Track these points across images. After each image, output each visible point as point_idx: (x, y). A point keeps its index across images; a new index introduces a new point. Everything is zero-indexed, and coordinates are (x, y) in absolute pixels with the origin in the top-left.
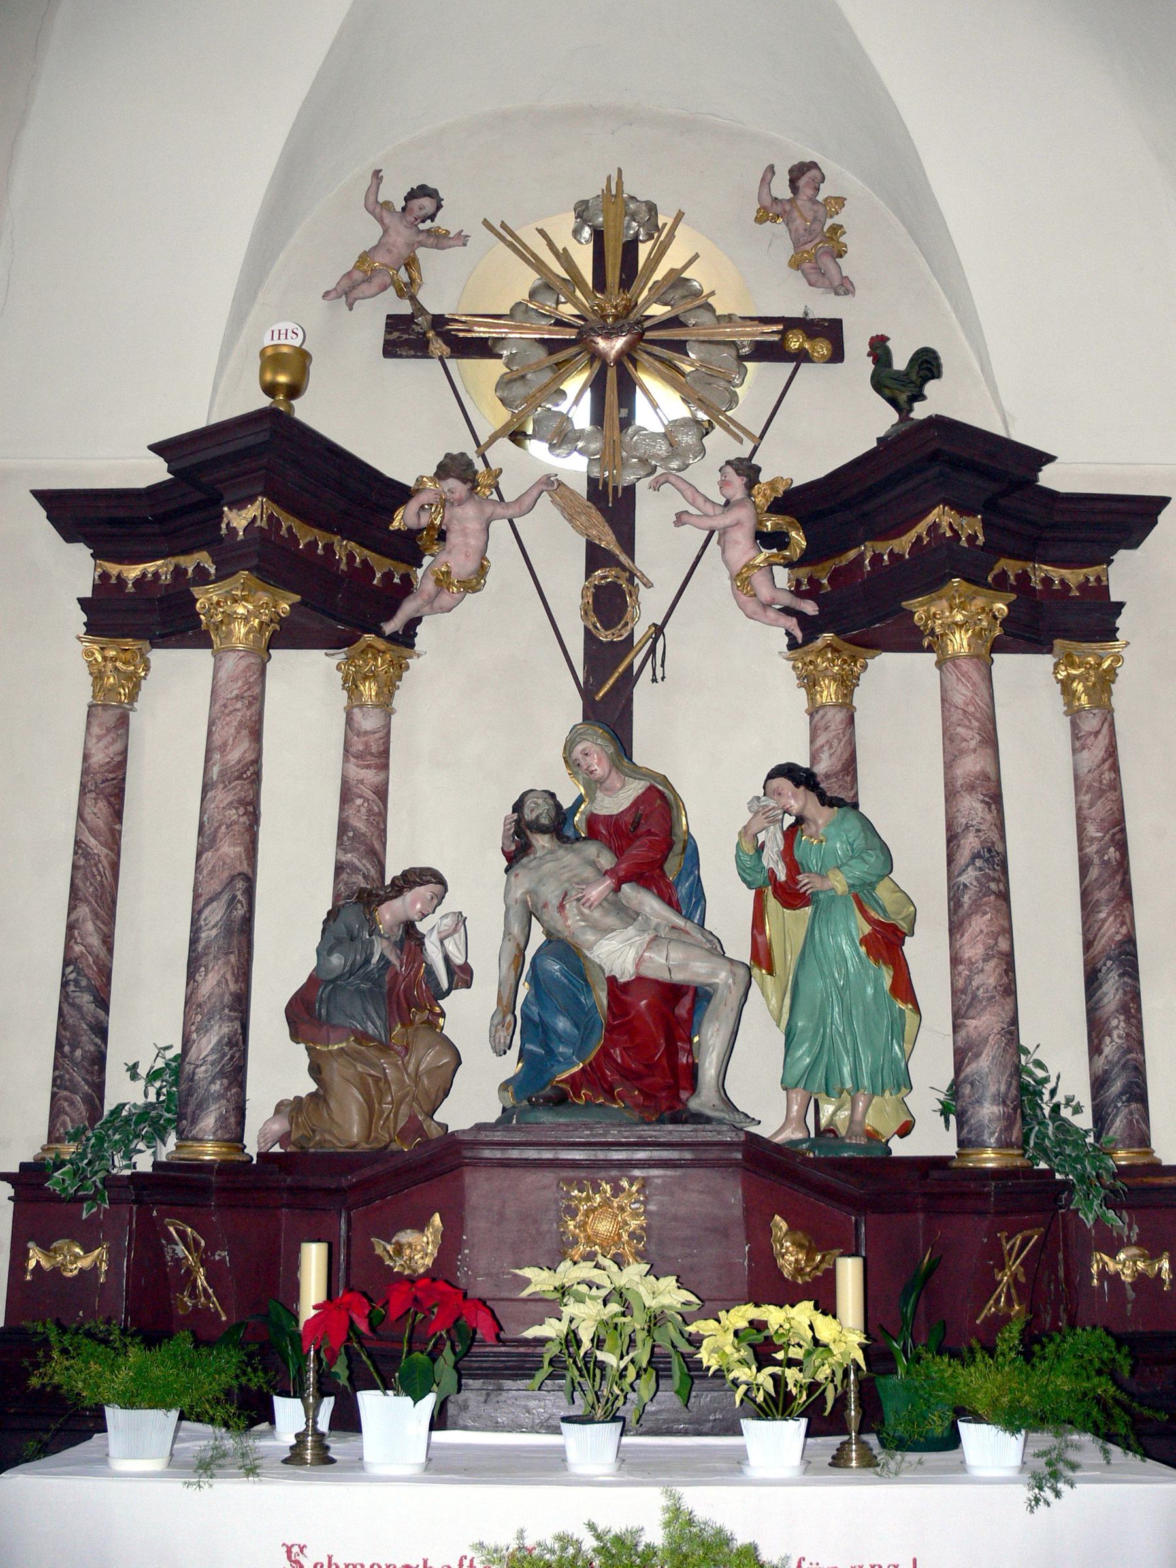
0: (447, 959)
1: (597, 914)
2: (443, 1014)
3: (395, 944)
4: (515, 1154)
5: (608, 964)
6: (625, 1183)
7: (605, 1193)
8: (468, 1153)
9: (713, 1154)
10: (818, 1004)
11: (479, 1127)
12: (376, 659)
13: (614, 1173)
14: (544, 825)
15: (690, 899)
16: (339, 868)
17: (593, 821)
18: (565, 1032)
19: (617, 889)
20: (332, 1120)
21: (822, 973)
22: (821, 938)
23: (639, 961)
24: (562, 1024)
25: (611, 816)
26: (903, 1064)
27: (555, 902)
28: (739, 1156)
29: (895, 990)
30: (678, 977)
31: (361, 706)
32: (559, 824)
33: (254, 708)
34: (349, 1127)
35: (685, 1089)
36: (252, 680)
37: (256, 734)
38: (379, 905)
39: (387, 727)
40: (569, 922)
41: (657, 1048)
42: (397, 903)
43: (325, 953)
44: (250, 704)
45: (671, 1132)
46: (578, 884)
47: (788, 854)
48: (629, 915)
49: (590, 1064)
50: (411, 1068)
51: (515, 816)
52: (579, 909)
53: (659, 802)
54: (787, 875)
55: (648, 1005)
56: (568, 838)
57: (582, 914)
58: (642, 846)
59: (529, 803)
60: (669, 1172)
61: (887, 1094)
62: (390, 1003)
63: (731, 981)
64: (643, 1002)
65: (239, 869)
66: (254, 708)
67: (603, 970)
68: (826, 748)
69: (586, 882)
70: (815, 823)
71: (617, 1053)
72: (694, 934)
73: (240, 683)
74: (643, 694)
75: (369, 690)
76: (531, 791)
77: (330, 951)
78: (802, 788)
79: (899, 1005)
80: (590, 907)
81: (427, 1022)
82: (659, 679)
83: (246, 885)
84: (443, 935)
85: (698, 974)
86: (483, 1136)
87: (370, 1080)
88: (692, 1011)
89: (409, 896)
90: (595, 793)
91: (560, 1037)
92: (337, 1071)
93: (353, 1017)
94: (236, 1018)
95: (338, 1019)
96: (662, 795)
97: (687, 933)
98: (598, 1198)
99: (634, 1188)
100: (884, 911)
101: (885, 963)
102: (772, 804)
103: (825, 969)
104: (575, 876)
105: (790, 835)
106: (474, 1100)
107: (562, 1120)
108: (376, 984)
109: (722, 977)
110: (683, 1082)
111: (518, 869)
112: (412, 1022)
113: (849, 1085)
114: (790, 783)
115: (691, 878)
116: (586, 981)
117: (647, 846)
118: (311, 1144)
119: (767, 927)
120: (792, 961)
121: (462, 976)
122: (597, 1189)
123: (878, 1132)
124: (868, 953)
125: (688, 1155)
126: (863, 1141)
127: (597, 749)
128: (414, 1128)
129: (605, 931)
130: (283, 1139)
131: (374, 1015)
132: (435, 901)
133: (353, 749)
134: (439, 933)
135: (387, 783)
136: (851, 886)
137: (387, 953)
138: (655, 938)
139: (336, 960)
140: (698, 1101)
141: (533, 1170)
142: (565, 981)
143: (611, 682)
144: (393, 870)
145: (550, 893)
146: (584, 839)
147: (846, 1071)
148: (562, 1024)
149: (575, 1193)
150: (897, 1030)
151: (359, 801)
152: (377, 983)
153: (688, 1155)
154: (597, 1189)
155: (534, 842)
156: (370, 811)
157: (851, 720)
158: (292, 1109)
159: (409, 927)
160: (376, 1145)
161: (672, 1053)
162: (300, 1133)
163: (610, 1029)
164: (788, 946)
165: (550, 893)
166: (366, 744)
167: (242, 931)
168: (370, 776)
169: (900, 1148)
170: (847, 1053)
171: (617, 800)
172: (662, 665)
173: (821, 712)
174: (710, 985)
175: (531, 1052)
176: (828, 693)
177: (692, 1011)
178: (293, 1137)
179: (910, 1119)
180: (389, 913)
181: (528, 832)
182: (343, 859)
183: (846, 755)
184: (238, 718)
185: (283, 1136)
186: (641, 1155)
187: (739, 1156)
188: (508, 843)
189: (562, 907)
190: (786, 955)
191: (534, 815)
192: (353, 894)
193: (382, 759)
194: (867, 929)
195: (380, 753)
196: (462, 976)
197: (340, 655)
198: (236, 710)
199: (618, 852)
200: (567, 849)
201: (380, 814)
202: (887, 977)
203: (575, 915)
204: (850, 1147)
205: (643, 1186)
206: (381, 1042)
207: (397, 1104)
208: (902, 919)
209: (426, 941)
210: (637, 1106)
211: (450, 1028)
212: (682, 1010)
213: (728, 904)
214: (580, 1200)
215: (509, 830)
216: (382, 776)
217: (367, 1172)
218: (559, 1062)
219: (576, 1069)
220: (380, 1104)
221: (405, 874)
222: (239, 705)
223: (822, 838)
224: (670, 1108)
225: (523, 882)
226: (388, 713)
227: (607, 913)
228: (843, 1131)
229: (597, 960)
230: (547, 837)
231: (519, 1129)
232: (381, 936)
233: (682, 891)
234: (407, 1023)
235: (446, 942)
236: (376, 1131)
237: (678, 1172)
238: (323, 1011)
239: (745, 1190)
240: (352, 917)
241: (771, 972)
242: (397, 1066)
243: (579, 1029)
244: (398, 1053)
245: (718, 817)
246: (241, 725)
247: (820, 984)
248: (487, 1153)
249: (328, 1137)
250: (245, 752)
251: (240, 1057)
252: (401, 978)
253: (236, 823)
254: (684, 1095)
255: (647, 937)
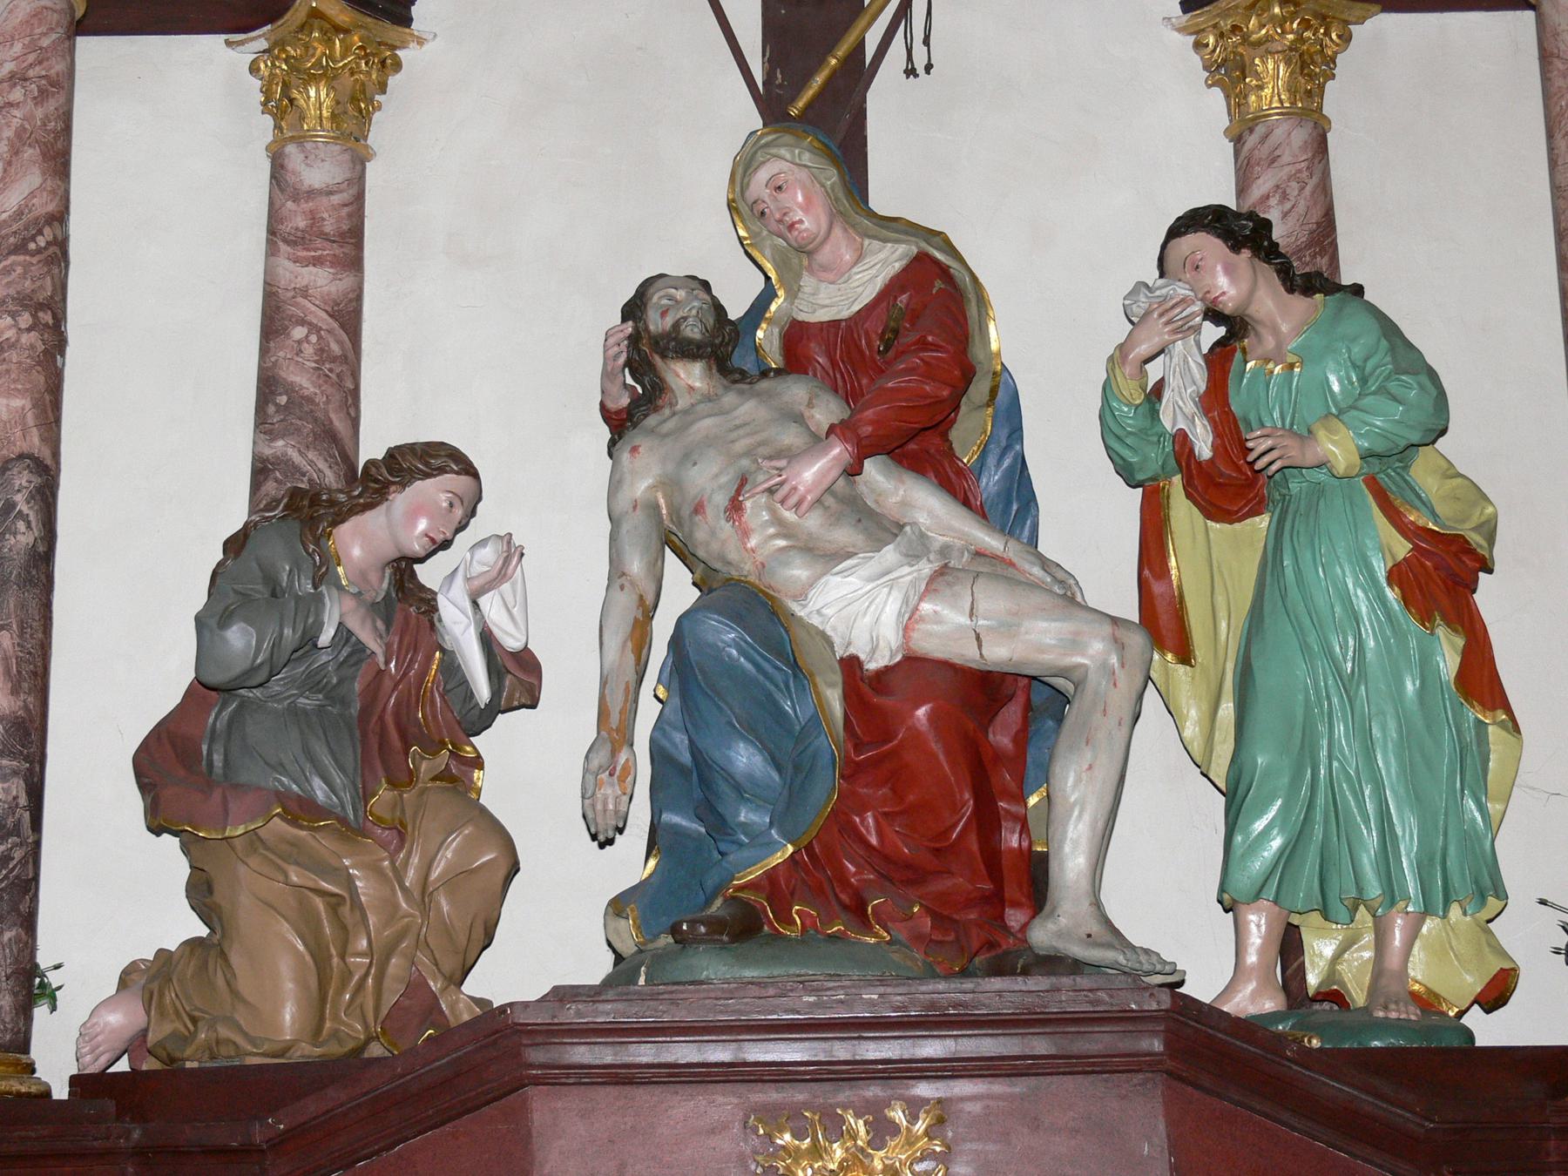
0: (487, 640)
1: (813, 522)
2: (478, 762)
3: (373, 607)
4: (645, 1053)
5: (841, 628)
6: (898, 1115)
7: (854, 1137)
8: (537, 1055)
9: (1097, 1042)
10: (1300, 718)
11: (562, 995)
12: (329, 43)
13: (873, 1091)
14: (690, 341)
15: (1008, 504)
16: (261, 471)
17: (796, 336)
18: (750, 776)
19: (853, 471)
20: (234, 992)
21: (1305, 648)
22: (1298, 572)
23: (910, 622)
24: (745, 758)
25: (835, 323)
26: (1488, 843)
27: (721, 499)
28: (1157, 1045)
29: (1463, 677)
30: (998, 654)
31: (300, 140)
32: (721, 344)
33: (52, 105)
34: (279, 1013)
35: (1016, 904)
36: (45, 42)
37: (58, 161)
38: (335, 523)
39: (358, 181)
40: (753, 542)
41: (956, 808)
42: (373, 520)
43: (213, 622)
44: (42, 96)
45: (999, 993)
46: (770, 458)
47: (1215, 401)
48: (882, 528)
49: (809, 848)
50: (411, 877)
51: (629, 327)
52: (773, 512)
53: (938, 284)
54: (1214, 447)
55: (931, 717)
56: (743, 373)
57: (778, 521)
58: (911, 371)
59: (657, 298)
60: (998, 1087)
61: (1455, 912)
62: (364, 735)
63: (1114, 660)
64: (922, 712)
65: (21, 446)
66: (52, 105)
67: (829, 642)
68: (1273, 201)
69: (791, 455)
70: (1275, 331)
71: (868, 825)
72: (1027, 567)
73: (18, 48)
74: (886, 101)
75: (317, 98)
76: (661, 276)
77: (225, 620)
78: (1246, 254)
79: (1473, 714)
80: (798, 505)
81: (444, 776)
82: (920, 69)
83: (37, 480)
84: (476, 583)
85: (1041, 649)
86: (571, 1014)
87: (319, 903)
88: (1022, 739)
89: (401, 500)
90: (799, 276)
91: (738, 788)
92: (248, 886)
93: (281, 768)
94: (15, 773)
95: (251, 773)
96: (944, 271)
97: (1012, 564)
98: (838, 1152)
99: (920, 1127)
100: (1434, 514)
101: (1448, 623)
102: (1182, 291)
103: (1312, 639)
104: (760, 444)
105: (1219, 360)
106: (552, 936)
107: (749, 973)
108: (332, 706)
109: (1094, 651)
110: (1011, 891)
111: (634, 437)
112: (412, 777)
113: (1374, 890)
114: (1218, 242)
115: (1007, 463)
116: (795, 665)
117: (912, 384)
118: (188, 1052)
119: (1173, 563)
120: (1229, 631)
121: (518, 678)
122: (836, 1128)
123: (1437, 996)
124: (1406, 601)
125: (1041, 1046)
126: (1413, 1014)
127: (803, 175)
128: (420, 1005)
129: (831, 558)
130: (136, 1045)
131: (327, 760)
132: (459, 512)
133: (287, 227)
134: (468, 580)
135: (359, 298)
136: (1366, 456)
137: (353, 624)
138: (943, 571)
139: (238, 638)
140: (1051, 926)
141: (688, 1089)
142: (749, 666)
143: (819, 80)
144: (371, 448)
145: (708, 478)
146: (778, 372)
147: (1367, 861)
148: (745, 758)
149: (787, 1138)
150: (1472, 766)
151: (299, 332)
152: (334, 695)
153: (1041, 1046)
154: (836, 1128)
155: (670, 379)
156: (321, 351)
157: (1320, 146)
158: (150, 979)
159: (403, 568)
160: (335, 1049)
161: (987, 821)
162: (167, 1028)
163: (852, 771)
164: (1220, 600)
165: (708, 478)
166: (313, 217)
167: (27, 581)
168: (322, 280)
169: (1489, 1030)
170: (1367, 821)
171: (849, 285)
172: (926, 42)
173: (1260, 130)
174: (1064, 673)
175: (676, 830)
176: (1273, 79)
177: (1022, 739)
178: (152, 1038)
179: (1507, 966)
180: (359, 543)
181: (657, 359)
182: (268, 452)
183: (1316, 215)
184: (16, 122)
185: (132, 1040)
186: (932, 1048)
187: (1157, 1045)
188: (615, 389)
189: (735, 507)
190: (1217, 624)
191: (669, 321)
192: (279, 502)
193: (348, 248)
194: (1402, 548)
195: (342, 235)
196: (518, 678)
197: (258, 41)
198: (10, 105)
199: (851, 396)
200: (741, 393)
201: (344, 359)
202: (1448, 656)
203: (765, 525)
204: (1386, 1026)
205: (941, 1121)
206: (343, 821)
207: (381, 957)
208: (1474, 529)
209: (442, 601)
210: (918, 938)
211: (496, 789)
212: (1001, 738)
213: (1088, 519)
214: (796, 1155)
215: (616, 357)
216: (347, 282)
217: (311, 1107)
218: (741, 845)
219: (778, 858)
220: (343, 957)
221: (393, 455)
222: (17, 94)
223: (1291, 358)
224: (991, 945)
225: (645, 473)
226: (360, 161)
227: (835, 519)
228: (1358, 997)
229: (815, 621)
230: (697, 368)
231: (654, 997)
232: (340, 588)
233: (990, 482)
234: (402, 779)
235: (483, 601)
236: (336, 1018)
237: (1019, 1087)
238: (218, 759)
239: (1171, 1123)
240: (278, 554)
241: (1185, 656)
242: (380, 872)
243: (779, 768)
244: (384, 845)
245: (1062, 329)
246: (21, 139)
247: (1301, 669)
248: (582, 1054)
249: (224, 1032)
250: (32, 194)
251: (23, 862)
252: (387, 684)
253: (13, 346)
254: (1014, 918)
255: (926, 568)
